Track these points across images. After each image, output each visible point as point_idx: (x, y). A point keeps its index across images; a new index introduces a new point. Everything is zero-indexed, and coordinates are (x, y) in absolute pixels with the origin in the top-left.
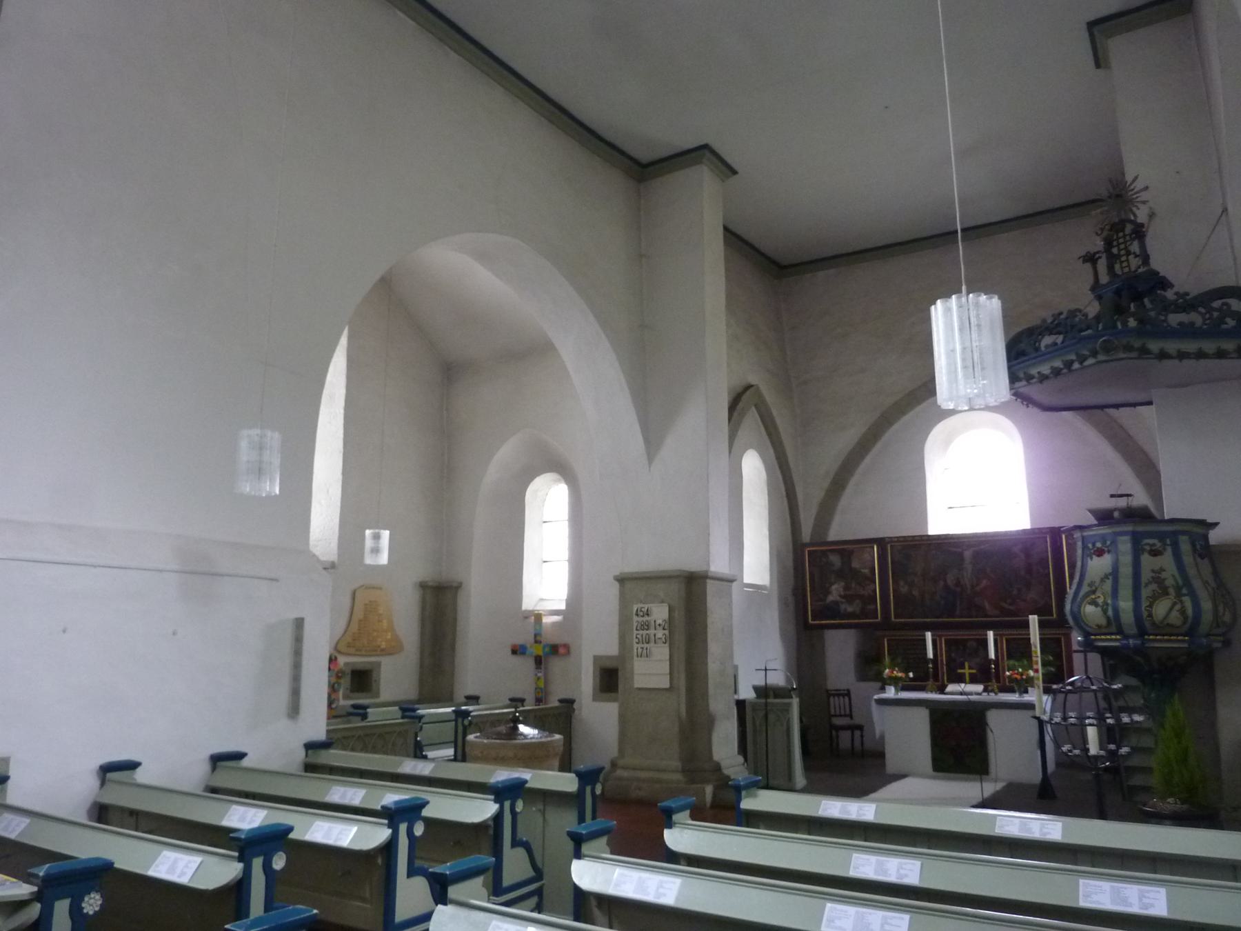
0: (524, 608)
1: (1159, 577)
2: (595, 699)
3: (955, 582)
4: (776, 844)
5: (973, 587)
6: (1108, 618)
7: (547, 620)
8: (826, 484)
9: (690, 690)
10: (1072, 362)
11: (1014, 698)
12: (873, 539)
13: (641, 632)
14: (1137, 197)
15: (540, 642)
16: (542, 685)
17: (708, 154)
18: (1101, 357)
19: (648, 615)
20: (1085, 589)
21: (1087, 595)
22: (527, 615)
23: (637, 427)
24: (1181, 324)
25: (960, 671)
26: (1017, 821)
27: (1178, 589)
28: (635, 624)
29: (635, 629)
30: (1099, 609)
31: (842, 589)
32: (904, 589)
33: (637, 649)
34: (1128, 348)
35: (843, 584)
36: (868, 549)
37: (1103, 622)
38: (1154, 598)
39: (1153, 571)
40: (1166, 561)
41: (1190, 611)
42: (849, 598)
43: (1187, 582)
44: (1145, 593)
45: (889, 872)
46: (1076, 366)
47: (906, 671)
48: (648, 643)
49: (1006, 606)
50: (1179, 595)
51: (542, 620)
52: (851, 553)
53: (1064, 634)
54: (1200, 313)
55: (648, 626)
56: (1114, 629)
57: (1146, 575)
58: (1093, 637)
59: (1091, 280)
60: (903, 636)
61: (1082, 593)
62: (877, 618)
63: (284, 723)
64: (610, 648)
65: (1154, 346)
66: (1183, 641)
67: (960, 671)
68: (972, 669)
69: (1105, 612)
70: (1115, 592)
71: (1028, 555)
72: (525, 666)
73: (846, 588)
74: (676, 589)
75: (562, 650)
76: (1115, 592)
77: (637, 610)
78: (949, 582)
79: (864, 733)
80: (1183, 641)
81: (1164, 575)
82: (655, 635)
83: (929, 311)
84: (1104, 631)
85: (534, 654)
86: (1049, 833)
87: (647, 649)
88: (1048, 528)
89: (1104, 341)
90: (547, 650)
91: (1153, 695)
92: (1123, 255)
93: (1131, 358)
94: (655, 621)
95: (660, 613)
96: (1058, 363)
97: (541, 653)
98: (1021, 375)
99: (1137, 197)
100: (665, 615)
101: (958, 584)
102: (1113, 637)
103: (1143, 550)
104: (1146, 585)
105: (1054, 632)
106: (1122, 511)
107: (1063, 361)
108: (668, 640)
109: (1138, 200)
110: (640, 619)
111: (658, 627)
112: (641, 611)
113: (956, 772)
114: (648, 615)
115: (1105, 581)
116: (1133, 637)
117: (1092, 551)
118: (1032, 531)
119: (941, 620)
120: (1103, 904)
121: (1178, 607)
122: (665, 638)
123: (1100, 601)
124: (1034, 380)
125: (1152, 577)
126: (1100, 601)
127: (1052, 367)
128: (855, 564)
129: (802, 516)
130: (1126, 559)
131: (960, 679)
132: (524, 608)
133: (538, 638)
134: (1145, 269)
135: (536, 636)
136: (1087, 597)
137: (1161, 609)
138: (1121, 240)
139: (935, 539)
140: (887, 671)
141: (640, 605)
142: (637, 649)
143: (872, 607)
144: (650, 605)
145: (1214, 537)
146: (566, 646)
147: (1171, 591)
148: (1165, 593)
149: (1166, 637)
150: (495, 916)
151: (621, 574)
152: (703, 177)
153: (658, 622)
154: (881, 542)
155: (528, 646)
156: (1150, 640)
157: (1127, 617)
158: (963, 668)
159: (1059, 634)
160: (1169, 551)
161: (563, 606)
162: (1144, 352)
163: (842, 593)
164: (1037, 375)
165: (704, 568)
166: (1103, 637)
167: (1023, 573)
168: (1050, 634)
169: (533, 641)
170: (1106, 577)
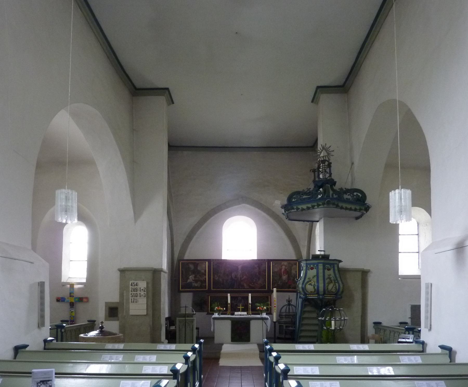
0: (62, 281)
1: (330, 277)
3: (235, 276)
5: (241, 278)
6: (315, 289)
7: (76, 287)
8: (185, 237)
9: (153, 315)
10: (314, 206)
12: (206, 259)
13: (133, 292)
14: (330, 153)
15: (73, 296)
16: (73, 314)
17: (167, 92)
19: (137, 285)
20: (307, 280)
21: (308, 282)
22: (64, 284)
23: (131, 206)
24: (347, 198)
25: (243, 307)
27: (334, 281)
28: (130, 289)
29: (130, 291)
30: (312, 286)
31: (193, 278)
32: (217, 278)
33: (132, 299)
34: (334, 204)
35: (194, 275)
36: (205, 263)
37: (313, 290)
38: (329, 283)
39: (328, 275)
40: (331, 272)
41: (337, 288)
42: (196, 281)
43: (337, 279)
44: (327, 281)
46: (316, 207)
47: (223, 308)
48: (137, 297)
49: (251, 285)
50: (335, 283)
51: (74, 287)
52: (198, 264)
53: (270, 295)
54: (351, 196)
55: (137, 290)
56: (316, 293)
57: (326, 276)
58: (308, 295)
59: (313, 178)
60: (244, 295)
61: (306, 282)
63: (37, 330)
64: (114, 298)
65: (340, 204)
66: (316, 296)
67: (243, 307)
69: (314, 287)
70: (318, 281)
71: (259, 267)
72: (65, 307)
73: (195, 277)
74: (149, 275)
75: (85, 300)
76: (318, 281)
77: (132, 283)
78: (233, 276)
79: (199, 330)
80: (316, 296)
81: (331, 276)
82: (140, 294)
83: (389, 194)
84: (313, 293)
85: (70, 302)
87: (136, 299)
89: (328, 200)
90: (77, 300)
92: (324, 172)
93: (333, 207)
94: (140, 288)
95: (142, 285)
96: (309, 205)
97: (73, 301)
98: (295, 207)
99: (330, 153)
100: (145, 286)
101: (236, 277)
102: (315, 295)
103: (326, 268)
104: (326, 280)
105: (260, 294)
106: (322, 255)
107: (311, 205)
108: (146, 296)
110: (133, 287)
111: (141, 290)
112: (134, 284)
113: (240, 341)
114: (137, 285)
116: (321, 295)
117: (310, 268)
119: (229, 289)
121: (335, 286)
122: (145, 295)
123: (313, 284)
124: (300, 210)
125: (328, 277)
126: (313, 284)
127: (307, 206)
129: (175, 248)
130: (321, 271)
132: (62, 281)
133: (72, 295)
134: (330, 178)
135: (70, 293)
136: (308, 283)
137: (330, 286)
138: (324, 167)
139: (224, 261)
140: (216, 308)
141: (133, 282)
142: (132, 299)
144: (137, 282)
145: (341, 265)
146: (87, 298)
147: (333, 282)
148: (332, 282)
149: (328, 295)
150: (309, 380)
151: (124, 268)
152: (161, 100)
154: (209, 261)
155: (66, 298)
157: (321, 289)
158: (240, 306)
159: (268, 295)
160: (332, 270)
161: (84, 281)
162: (337, 206)
163: (194, 279)
164: (301, 208)
165: (160, 267)
167: (257, 274)
169: (69, 295)
170: (314, 276)
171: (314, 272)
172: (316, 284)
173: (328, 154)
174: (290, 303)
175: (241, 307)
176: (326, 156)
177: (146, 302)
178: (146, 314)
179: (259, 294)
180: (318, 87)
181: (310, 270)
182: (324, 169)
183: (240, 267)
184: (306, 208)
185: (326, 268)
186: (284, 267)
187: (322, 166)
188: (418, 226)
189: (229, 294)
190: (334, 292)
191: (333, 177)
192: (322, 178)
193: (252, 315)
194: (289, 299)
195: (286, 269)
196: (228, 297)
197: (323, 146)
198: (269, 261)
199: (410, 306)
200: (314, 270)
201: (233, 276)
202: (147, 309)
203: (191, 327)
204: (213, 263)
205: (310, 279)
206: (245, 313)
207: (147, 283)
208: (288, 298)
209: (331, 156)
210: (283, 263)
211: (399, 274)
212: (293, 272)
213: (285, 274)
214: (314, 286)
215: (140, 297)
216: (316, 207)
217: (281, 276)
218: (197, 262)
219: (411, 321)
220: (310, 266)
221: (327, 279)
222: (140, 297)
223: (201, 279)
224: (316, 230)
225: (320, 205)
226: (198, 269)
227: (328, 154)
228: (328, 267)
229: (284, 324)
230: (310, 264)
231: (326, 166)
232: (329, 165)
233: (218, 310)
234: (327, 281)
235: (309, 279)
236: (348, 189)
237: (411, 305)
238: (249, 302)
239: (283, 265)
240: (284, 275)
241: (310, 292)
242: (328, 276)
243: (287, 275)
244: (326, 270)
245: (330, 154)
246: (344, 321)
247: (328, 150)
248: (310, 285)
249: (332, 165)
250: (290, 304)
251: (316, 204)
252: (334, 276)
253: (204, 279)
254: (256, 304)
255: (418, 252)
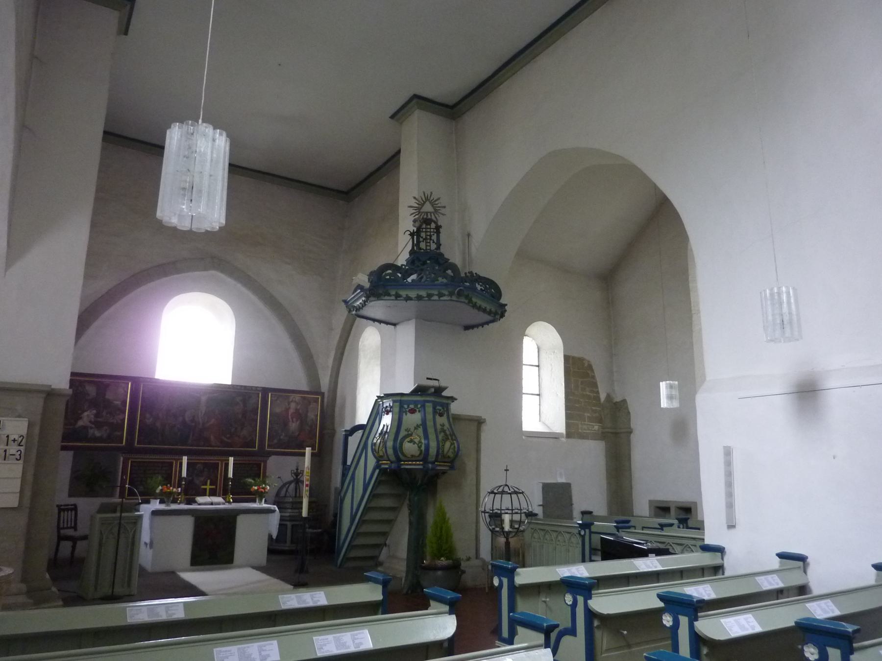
2: (651, 502)
4: (637, 595)
10: (432, 295)
11: (256, 506)
18: (454, 298)
20: (403, 433)
26: (146, 607)
30: (416, 445)
31: (93, 416)
34: (467, 297)
35: (95, 411)
37: (418, 453)
39: (441, 425)
42: (98, 425)
44: (440, 437)
45: (347, 644)
46: (436, 298)
49: (225, 439)
50: (452, 439)
53: (222, 461)
56: (421, 458)
57: (439, 427)
58: (403, 463)
62: (122, 443)
68: (203, 489)
69: (420, 447)
70: (426, 437)
73: (97, 415)
74: (38, 403)
76: (426, 437)
82: (5, 451)
86: (174, 614)
88: (261, 387)
91: (416, 498)
94: (8, 436)
99: (439, 210)
100: (24, 431)
104: (440, 434)
109: (439, 211)
111: (10, 442)
115: (418, 429)
117: (407, 410)
118: (231, 385)
120: (332, 651)
121: (452, 446)
122: (20, 455)
123: (417, 441)
128: (109, 396)
130: (429, 417)
131: (203, 493)
143: (119, 433)
148: (448, 439)
153: (11, 438)
156: (402, 464)
157: (433, 451)
159: (172, 459)
160: (445, 415)
163: (93, 420)
166: (410, 463)
167: (240, 416)
168: (239, 460)
171: (417, 418)
172: (423, 441)
173: (436, 211)
174: (299, 477)
175: (208, 487)
176: (431, 213)
177: (20, 475)
178: (16, 505)
179: (240, 459)
180: (416, 96)
181: (408, 414)
182: (429, 234)
183: (204, 399)
184: (416, 296)
185: (437, 412)
186: (293, 405)
187: (426, 228)
188: (538, 352)
189: (186, 457)
190: (409, 457)
191: (442, 250)
192: (425, 248)
193: (233, 502)
194: (297, 469)
195: (297, 410)
196: (230, 464)
197: (426, 195)
198: (265, 391)
199: (541, 485)
200: (416, 413)
201: (187, 419)
202: (22, 492)
203: (131, 536)
204: (143, 385)
205: (409, 431)
206: (219, 499)
207: (30, 426)
208: (296, 468)
209: (441, 216)
210: (293, 396)
211: (523, 430)
212: (311, 415)
213: (294, 419)
214: (420, 444)
215: (5, 460)
216: (436, 298)
217: (286, 424)
218: (107, 381)
219: (544, 512)
220: (408, 407)
221: (440, 432)
222: (5, 460)
223: (112, 421)
224: (361, 340)
225: (444, 295)
226: (107, 397)
227: (436, 211)
228: (440, 410)
229: (290, 521)
230: (409, 403)
231: (432, 230)
232: (438, 228)
233: (165, 492)
234: (441, 436)
235: (408, 432)
236: (479, 276)
237: (542, 483)
238: (229, 476)
239: (292, 401)
240: (293, 421)
241: (409, 456)
242: (440, 427)
243: (298, 422)
244: (438, 415)
245: (439, 211)
246: (519, 515)
247: (435, 204)
248: (411, 443)
249: (441, 230)
250: (299, 479)
251: (436, 292)
252: (449, 428)
253: (119, 422)
254: (247, 479)
255: (539, 395)
